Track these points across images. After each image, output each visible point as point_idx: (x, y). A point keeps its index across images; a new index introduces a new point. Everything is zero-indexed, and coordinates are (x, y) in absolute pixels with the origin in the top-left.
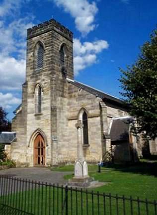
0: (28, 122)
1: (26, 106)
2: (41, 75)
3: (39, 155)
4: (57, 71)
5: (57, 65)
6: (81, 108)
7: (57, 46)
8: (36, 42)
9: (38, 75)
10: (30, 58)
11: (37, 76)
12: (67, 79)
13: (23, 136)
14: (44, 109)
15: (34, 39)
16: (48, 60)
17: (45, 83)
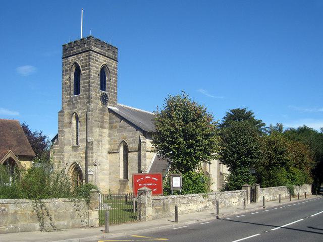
2: (77, 103)
5: (96, 92)
11: (74, 104)
15: (70, 59)
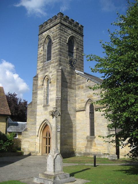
0: (38, 113)
1: (36, 97)
2: (49, 68)
3: (47, 145)
4: (64, 62)
5: (64, 57)
6: (88, 99)
7: (65, 38)
8: (46, 36)
9: (47, 67)
10: (41, 52)
11: (46, 69)
12: (76, 71)
13: (33, 126)
14: (51, 100)
15: (44, 34)
16: (55, 52)
17: (52, 75)
